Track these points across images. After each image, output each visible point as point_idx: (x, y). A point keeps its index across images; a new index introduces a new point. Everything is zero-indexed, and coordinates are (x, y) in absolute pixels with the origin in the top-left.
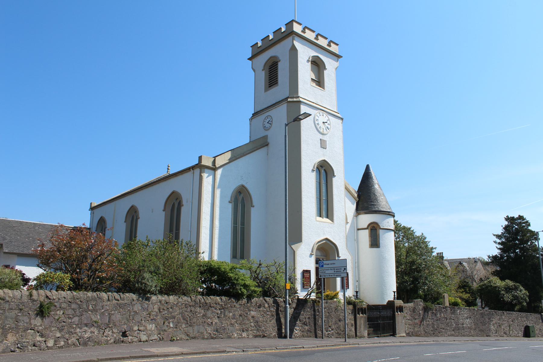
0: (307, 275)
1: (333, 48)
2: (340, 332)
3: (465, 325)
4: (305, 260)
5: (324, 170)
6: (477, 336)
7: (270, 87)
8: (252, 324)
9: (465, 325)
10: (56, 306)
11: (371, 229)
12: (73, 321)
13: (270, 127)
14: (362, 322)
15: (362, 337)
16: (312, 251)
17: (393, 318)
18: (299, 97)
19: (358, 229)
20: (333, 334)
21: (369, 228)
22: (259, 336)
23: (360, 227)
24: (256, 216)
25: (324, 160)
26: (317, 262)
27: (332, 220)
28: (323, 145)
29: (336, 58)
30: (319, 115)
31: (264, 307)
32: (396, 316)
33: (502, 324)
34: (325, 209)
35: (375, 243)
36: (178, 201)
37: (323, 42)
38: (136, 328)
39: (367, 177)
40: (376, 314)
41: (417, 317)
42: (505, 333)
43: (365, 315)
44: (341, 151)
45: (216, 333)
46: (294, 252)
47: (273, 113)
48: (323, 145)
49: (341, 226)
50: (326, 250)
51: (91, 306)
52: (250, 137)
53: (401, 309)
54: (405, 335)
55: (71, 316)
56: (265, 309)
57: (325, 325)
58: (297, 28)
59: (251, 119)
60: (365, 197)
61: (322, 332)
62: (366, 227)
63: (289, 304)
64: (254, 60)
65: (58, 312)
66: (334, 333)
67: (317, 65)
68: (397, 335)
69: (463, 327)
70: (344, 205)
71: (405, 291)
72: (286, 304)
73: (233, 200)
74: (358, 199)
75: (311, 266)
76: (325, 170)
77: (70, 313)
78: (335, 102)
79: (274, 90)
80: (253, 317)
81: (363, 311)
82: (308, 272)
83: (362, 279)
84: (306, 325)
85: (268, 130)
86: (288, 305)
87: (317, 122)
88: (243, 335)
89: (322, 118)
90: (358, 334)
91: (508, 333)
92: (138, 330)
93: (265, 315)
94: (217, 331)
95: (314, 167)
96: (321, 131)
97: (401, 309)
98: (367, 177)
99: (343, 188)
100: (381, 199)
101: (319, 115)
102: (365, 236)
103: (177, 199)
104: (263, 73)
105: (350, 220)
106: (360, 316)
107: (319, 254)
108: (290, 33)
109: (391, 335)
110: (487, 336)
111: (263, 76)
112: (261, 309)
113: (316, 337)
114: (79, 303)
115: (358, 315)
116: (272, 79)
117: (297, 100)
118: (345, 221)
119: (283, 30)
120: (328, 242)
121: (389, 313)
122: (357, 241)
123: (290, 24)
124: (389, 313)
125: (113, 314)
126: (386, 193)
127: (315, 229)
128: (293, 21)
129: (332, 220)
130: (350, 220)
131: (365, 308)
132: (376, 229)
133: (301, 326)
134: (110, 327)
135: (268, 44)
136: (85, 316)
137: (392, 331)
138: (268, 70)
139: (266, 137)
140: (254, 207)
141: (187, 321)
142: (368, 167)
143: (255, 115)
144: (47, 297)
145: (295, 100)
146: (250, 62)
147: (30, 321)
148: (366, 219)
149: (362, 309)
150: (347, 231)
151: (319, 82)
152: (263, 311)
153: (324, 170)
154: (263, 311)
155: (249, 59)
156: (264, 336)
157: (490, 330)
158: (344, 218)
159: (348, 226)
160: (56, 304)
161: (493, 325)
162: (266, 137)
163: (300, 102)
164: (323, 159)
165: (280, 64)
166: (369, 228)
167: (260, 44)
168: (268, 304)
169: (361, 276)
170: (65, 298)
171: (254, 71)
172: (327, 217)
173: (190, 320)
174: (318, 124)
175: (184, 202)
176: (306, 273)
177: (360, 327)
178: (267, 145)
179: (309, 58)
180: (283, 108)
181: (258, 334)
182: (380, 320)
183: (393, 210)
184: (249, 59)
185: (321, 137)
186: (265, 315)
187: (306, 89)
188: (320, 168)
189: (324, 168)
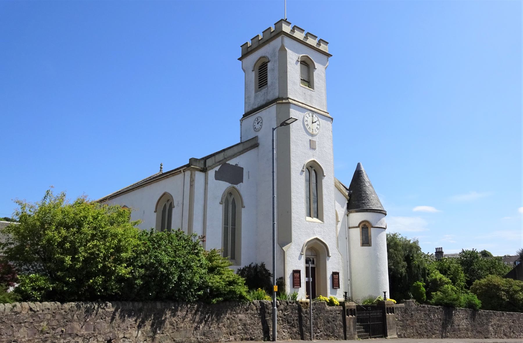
0: (297, 275)
1: (323, 47)
2: (328, 333)
3: (461, 327)
4: (295, 260)
5: (314, 171)
6: (475, 338)
7: (260, 88)
8: (240, 327)
9: (461, 327)
10: (39, 317)
11: (362, 228)
12: (57, 331)
13: (260, 129)
14: (352, 323)
15: (352, 338)
16: (302, 251)
17: (384, 319)
18: (288, 98)
19: (349, 228)
20: (321, 336)
21: (361, 226)
22: (247, 339)
23: (351, 226)
24: (246, 217)
25: (314, 161)
26: (307, 262)
27: (322, 220)
28: (312, 146)
29: (325, 57)
30: (308, 116)
31: (252, 309)
32: (387, 317)
33: (501, 326)
34: (315, 209)
35: (366, 241)
36: (169, 203)
37: (312, 42)
38: (121, 336)
39: (358, 176)
40: (365, 315)
41: (409, 318)
42: (505, 335)
43: (354, 316)
44: (331, 151)
45: (203, 337)
46: (284, 252)
47: (263, 114)
48: (312, 146)
49: (330, 225)
50: (316, 252)
51: (75, 316)
52: (241, 138)
53: (392, 310)
54: (396, 336)
55: (55, 327)
56: (252, 312)
57: (314, 327)
58: (287, 29)
59: (242, 120)
60: (356, 196)
61: (311, 334)
62: (357, 225)
63: (277, 306)
64: (244, 60)
65: (42, 324)
66: (323, 335)
67: (307, 65)
68: (389, 337)
69: (459, 328)
70: (334, 203)
71: (400, 285)
72: (273, 306)
73: (224, 201)
74: (348, 198)
75: (301, 266)
76: (314, 170)
77: (54, 324)
78: (324, 102)
79: (264, 90)
80: (240, 320)
81: (352, 312)
82: (299, 272)
83: (354, 278)
84: (294, 327)
85: (259, 131)
86: (276, 308)
87: (306, 123)
88: (231, 339)
89: (309, 117)
90: (347, 336)
91: (508, 334)
92: (124, 337)
93: (253, 318)
94: (204, 335)
95: (303, 168)
96: (311, 132)
97: (392, 310)
98: (358, 176)
99: (333, 188)
100: (372, 197)
101: (308, 116)
102: (356, 234)
103: (168, 201)
104: (254, 73)
105: (340, 219)
106: (349, 317)
107: (309, 253)
108: (279, 33)
109: (382, 337)
110: (486, 338)
111: (253, 76)
112: (249, 312)
113: (302, 339)
114: (64, 313)
115: (347, 317)
116: (262, 81)
117: (287, 101)
118: (335, 220)
119: (273, 29)
120: (319, 242)
121: (379, 314)
122: (348, 238)
123: (278, 24)
124: (379, 314)
125: (98, 323)
126: (377, 191)
127: (304, 229)
128: (282, 20)
129: (322, 220)
130: (340, 219)
131: (354, 309)
132: (367, 228)
133: (289, 328)
134: (94, 336)
135: (259, 43)
136: (69, 326)
137: (383, 334)
138: (258, 71)
139: (256, 138)
140: (244, 207)
141: (174, 326)
142: (359, 165)
143: (246, 115)
144: (31, 309)
145: (284, 101)
146: (240, 62)
147: (13, 333)
148: (357, 217)
149: (351, 310)
150: (339, 229)
151: (308, 81)
152: (251, 314)
153: (314, 171)
154: (251, 314)
155: (240, 59)
156: (252, 339)
157: (488, 331)
158: (335, 217)
159: (340, 225)
160: (39, 315)
161: (492, 326)
162: (256, 138)
163: (289, 103)
164: (313, 159)
165: (269, 65)
166: (361, 226)
167: (250, 44)
168: (256, 307)
169: (353, 275)
170: (49, 309)
171: (244, 71)
172: (317, 217)
173: (177, 325)
174: (307, 125)
175: (175, 204)
176: (296, 272)
177: (350, 329)
178: (257, 146)
179: (299, 59)
180: (273, 108)
181: (246, 336)
182: (371, 316)
183: (385, 209)
184: (240, 59)
185: (310, 138)
186: (253, 318)
187: (295, 90)
188: (310, 168)
189: (313, 169)
